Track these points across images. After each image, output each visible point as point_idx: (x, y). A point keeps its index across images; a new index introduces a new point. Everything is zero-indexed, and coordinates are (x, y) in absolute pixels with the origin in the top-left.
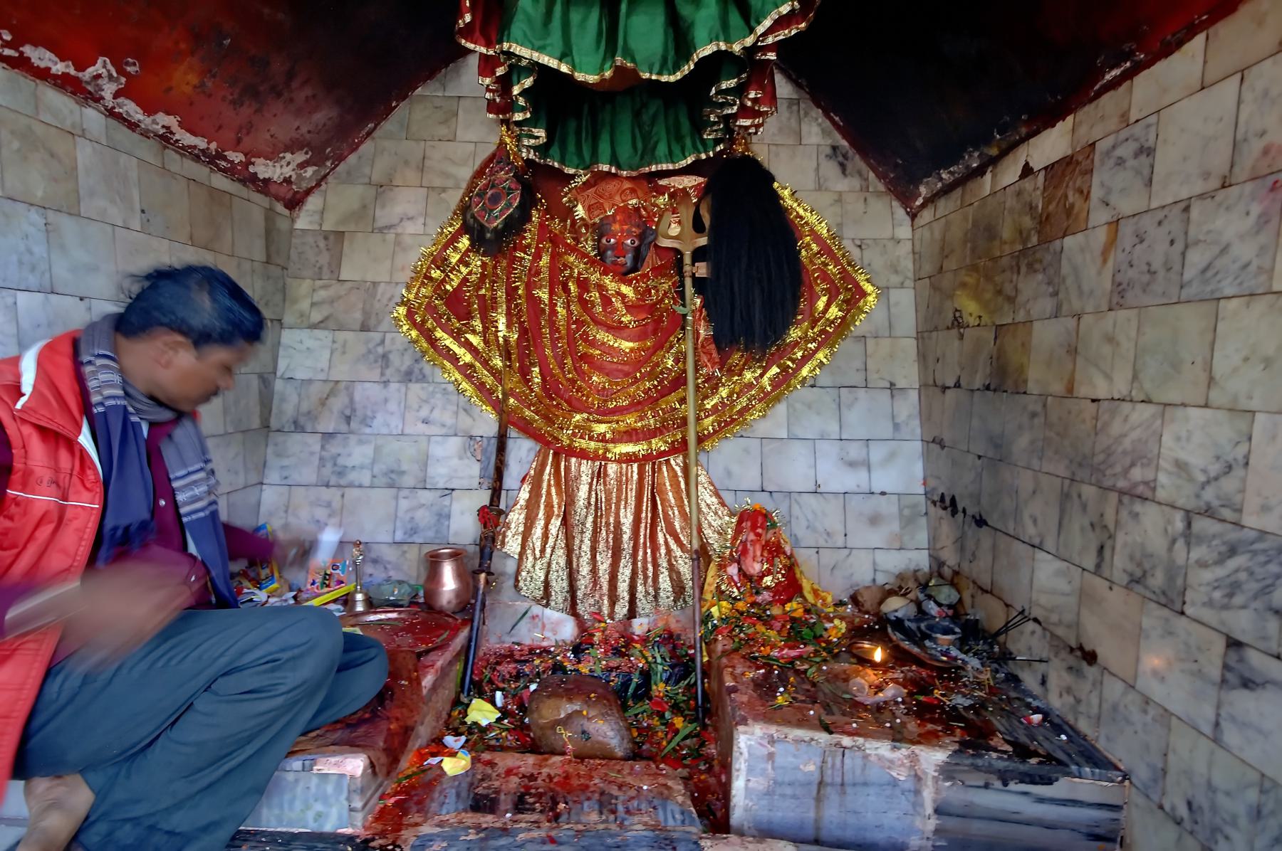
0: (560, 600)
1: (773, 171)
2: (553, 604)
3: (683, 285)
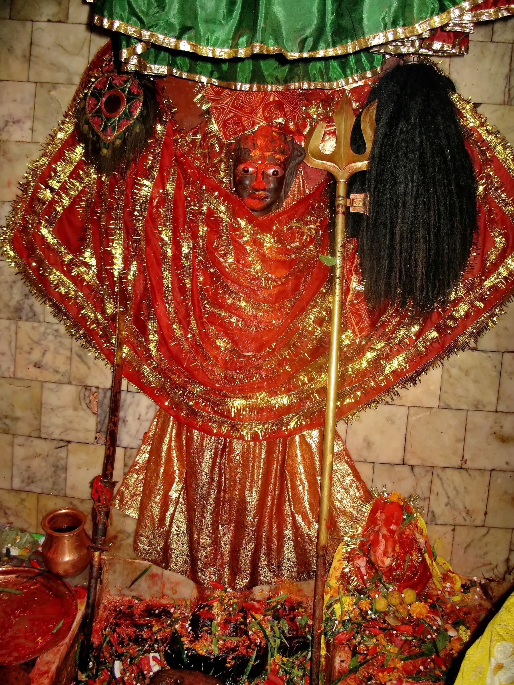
0: (181, 562)
1: (454, 77)
2: (173, 565)
3: (333, 225)
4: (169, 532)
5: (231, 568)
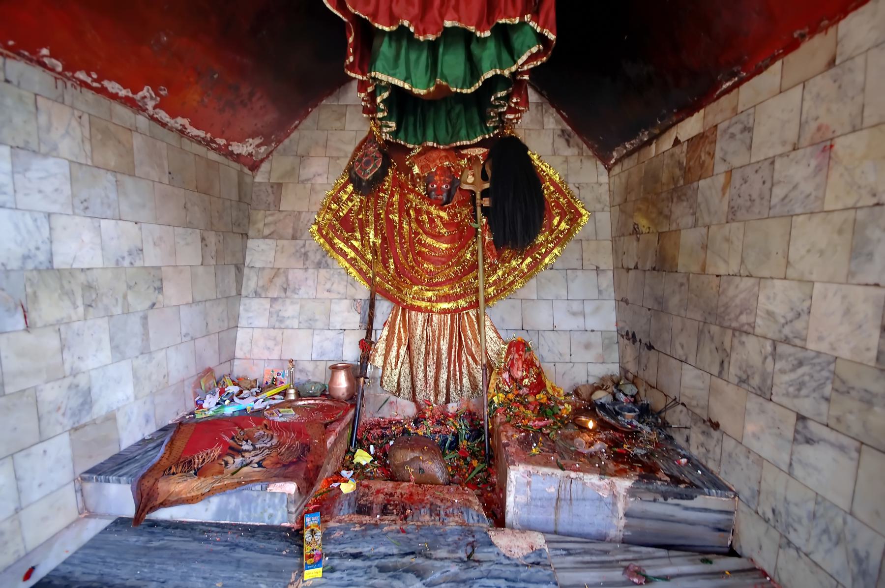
1: (527, 144)
5: (435, 391)
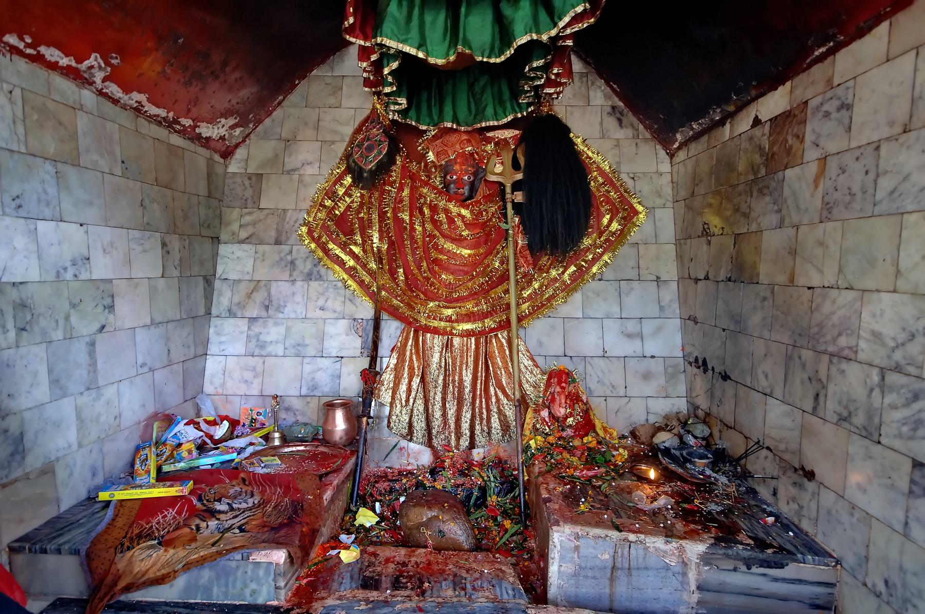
3: (505, 208)
4: (412, 410)
5: (456, 434)
